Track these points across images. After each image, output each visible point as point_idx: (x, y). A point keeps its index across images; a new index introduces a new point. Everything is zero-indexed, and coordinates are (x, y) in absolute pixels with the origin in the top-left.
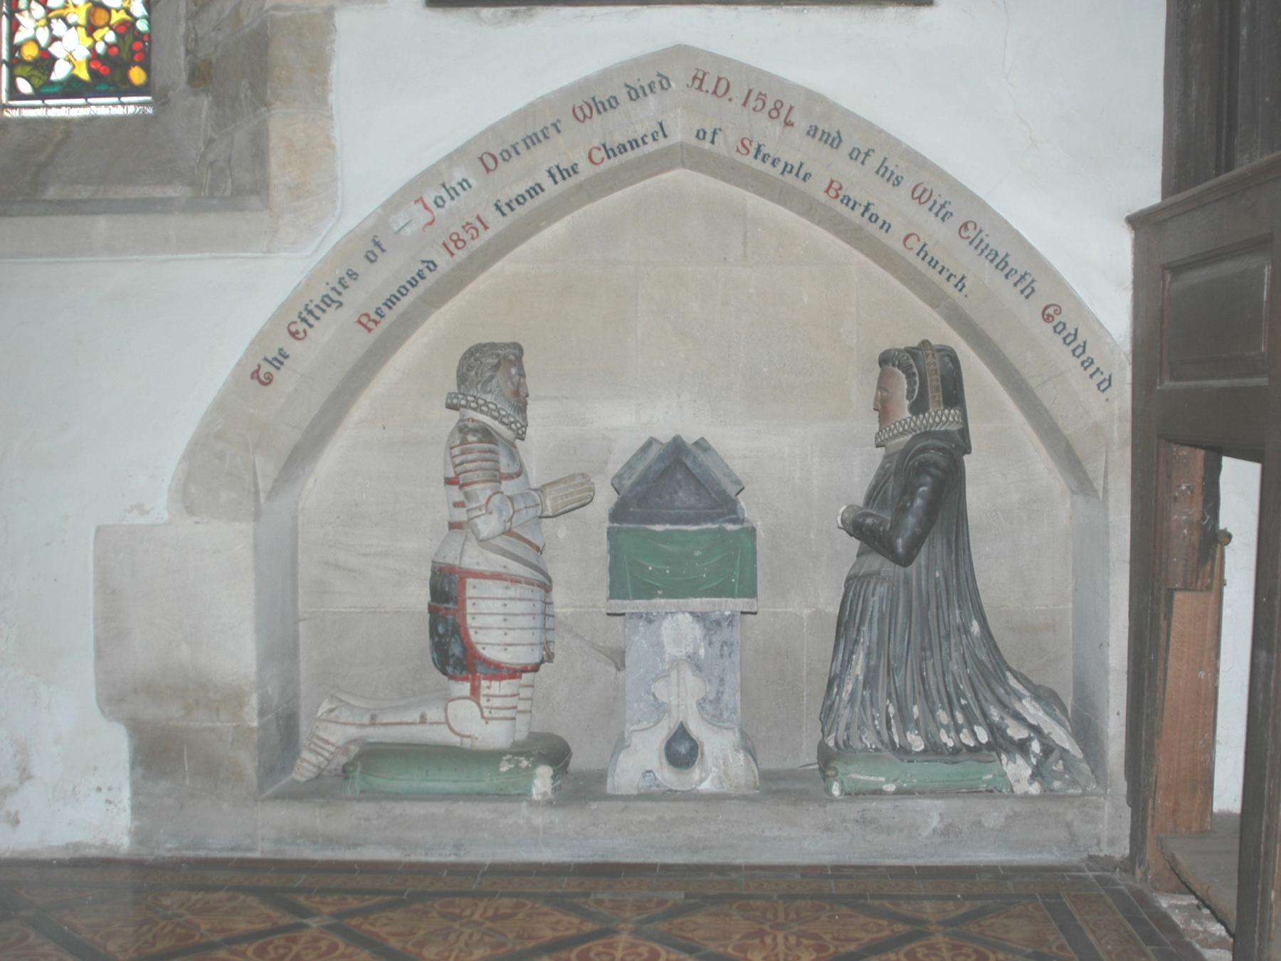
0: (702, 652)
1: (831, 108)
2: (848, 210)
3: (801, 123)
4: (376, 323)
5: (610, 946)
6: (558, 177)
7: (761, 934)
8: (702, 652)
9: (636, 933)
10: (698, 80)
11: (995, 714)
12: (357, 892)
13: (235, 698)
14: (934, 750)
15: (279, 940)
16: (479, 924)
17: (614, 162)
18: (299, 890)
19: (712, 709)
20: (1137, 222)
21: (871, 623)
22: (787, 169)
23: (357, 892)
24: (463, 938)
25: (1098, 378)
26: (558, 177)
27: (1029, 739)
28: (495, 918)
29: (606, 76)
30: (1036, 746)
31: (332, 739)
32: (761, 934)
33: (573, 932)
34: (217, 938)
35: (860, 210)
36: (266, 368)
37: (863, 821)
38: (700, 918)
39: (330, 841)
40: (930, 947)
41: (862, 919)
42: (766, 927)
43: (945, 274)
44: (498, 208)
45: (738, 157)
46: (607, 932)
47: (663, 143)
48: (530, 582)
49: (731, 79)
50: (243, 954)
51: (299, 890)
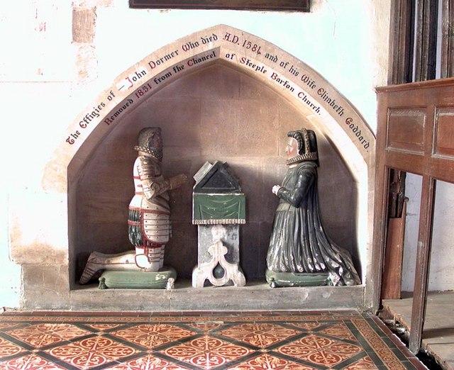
0: (226, 238)
1: (274, 47)
2: (207, 60)
3: (264, 53)
4: (111, 122)
5: (94, 340)
6: (177, 70)
7: (253, 335)
8: (226, 238)
9: (210, 335)
10: (227, 37)
11: (328, 259)
12: (9, 322)
13: (62, 255)
14: (306, 271)
15: (89, 340)
16: (152, 334)
17: (197, 65)
18: (89, 323)
19: (229, 258)
20: (379, 90)
21: (286, 228)
22: (258, 68)
23: (9, 322)
24: (45, 337)
25: (364, 144)
26: (177, 70)
27: (339, 267)
28: (161, 331)
29: (194, 35)
30: (341, 270)
31: (94, 269)
32: (253, 335)
33: (83, 335)
34: (68, 340)
35: (283, 83)
36: (72, 138)
37: (282, 295)
38: (231, 330)
39: (95, 305)
40: (310, 338)
41: (285, 329)
42: (254, 332)
43: (313, 106)
44: (155, 81)
45: (241, 64)
46: (200, 335)
47: (214, 58)
48: (166, 214)
49: (239, 37)
50: (79, 345)
51: (89, 323)
